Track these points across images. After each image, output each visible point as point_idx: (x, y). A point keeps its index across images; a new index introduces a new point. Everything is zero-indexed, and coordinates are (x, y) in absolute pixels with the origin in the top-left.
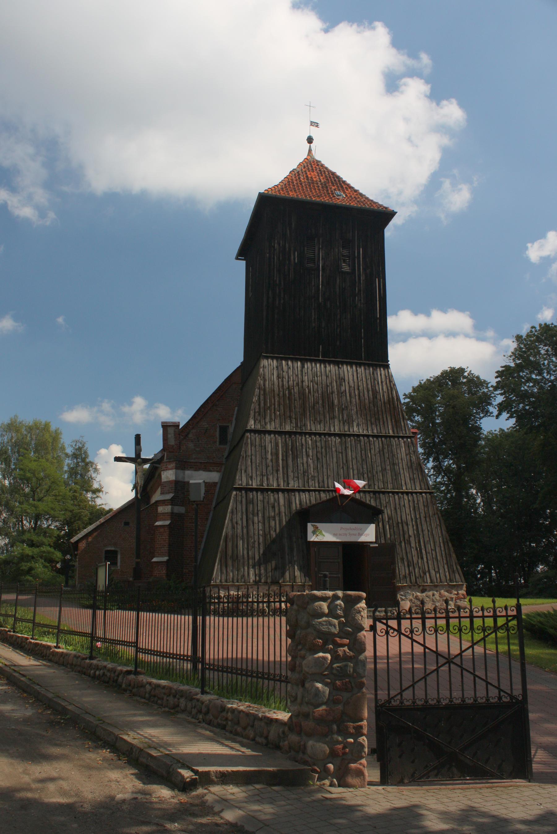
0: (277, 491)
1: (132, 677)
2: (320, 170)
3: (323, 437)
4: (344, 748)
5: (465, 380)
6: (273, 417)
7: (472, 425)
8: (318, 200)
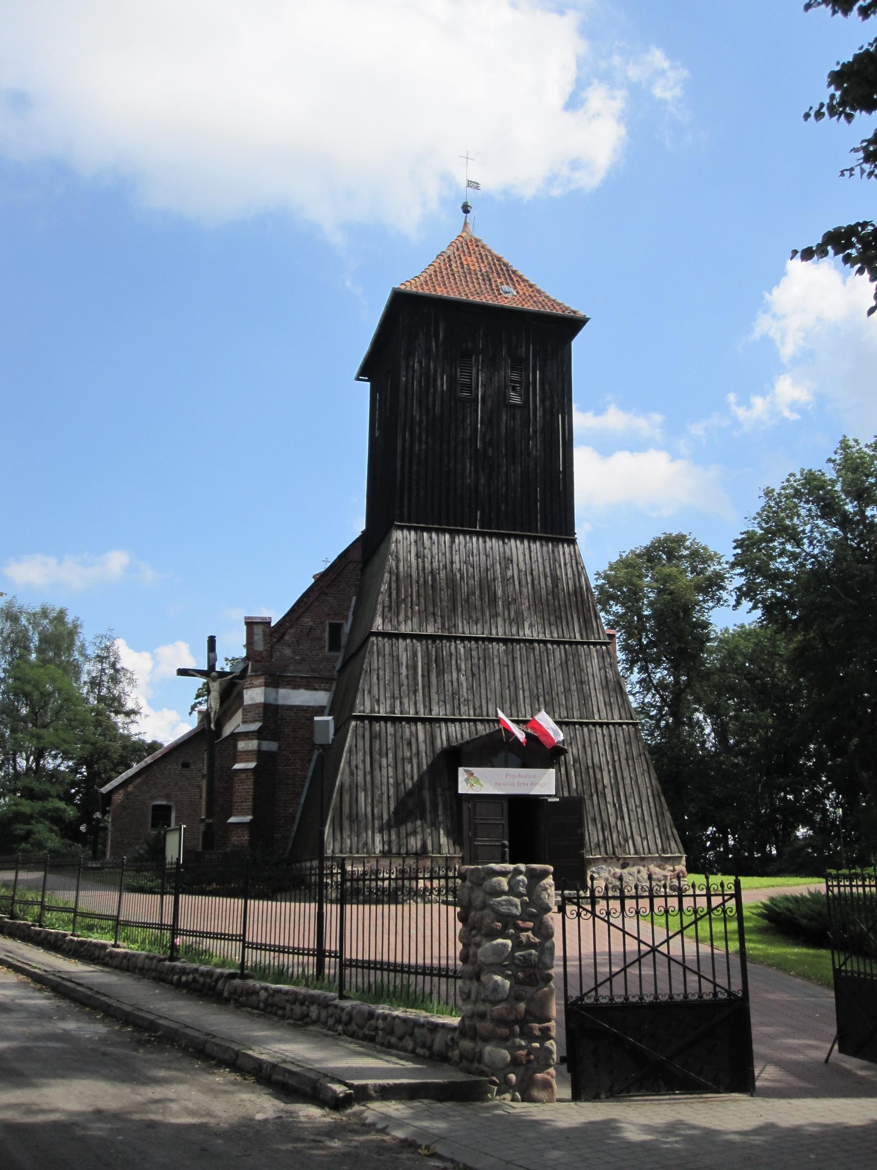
0: (415, 720)
1: (237, 982)
2: (480, 254)
3: (480, 643)
4: (528, 1054)
5: (687, 552)
6: (410, 614)
7: (698, 619)
8: (478, 299)
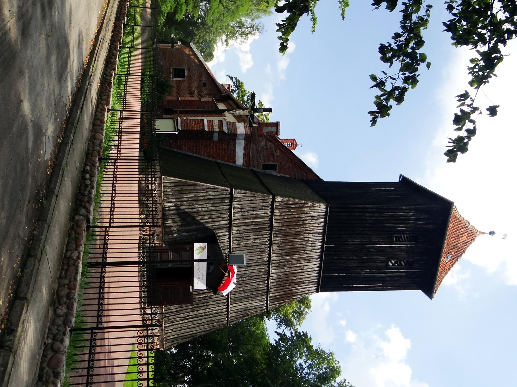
0: (230, 219)
